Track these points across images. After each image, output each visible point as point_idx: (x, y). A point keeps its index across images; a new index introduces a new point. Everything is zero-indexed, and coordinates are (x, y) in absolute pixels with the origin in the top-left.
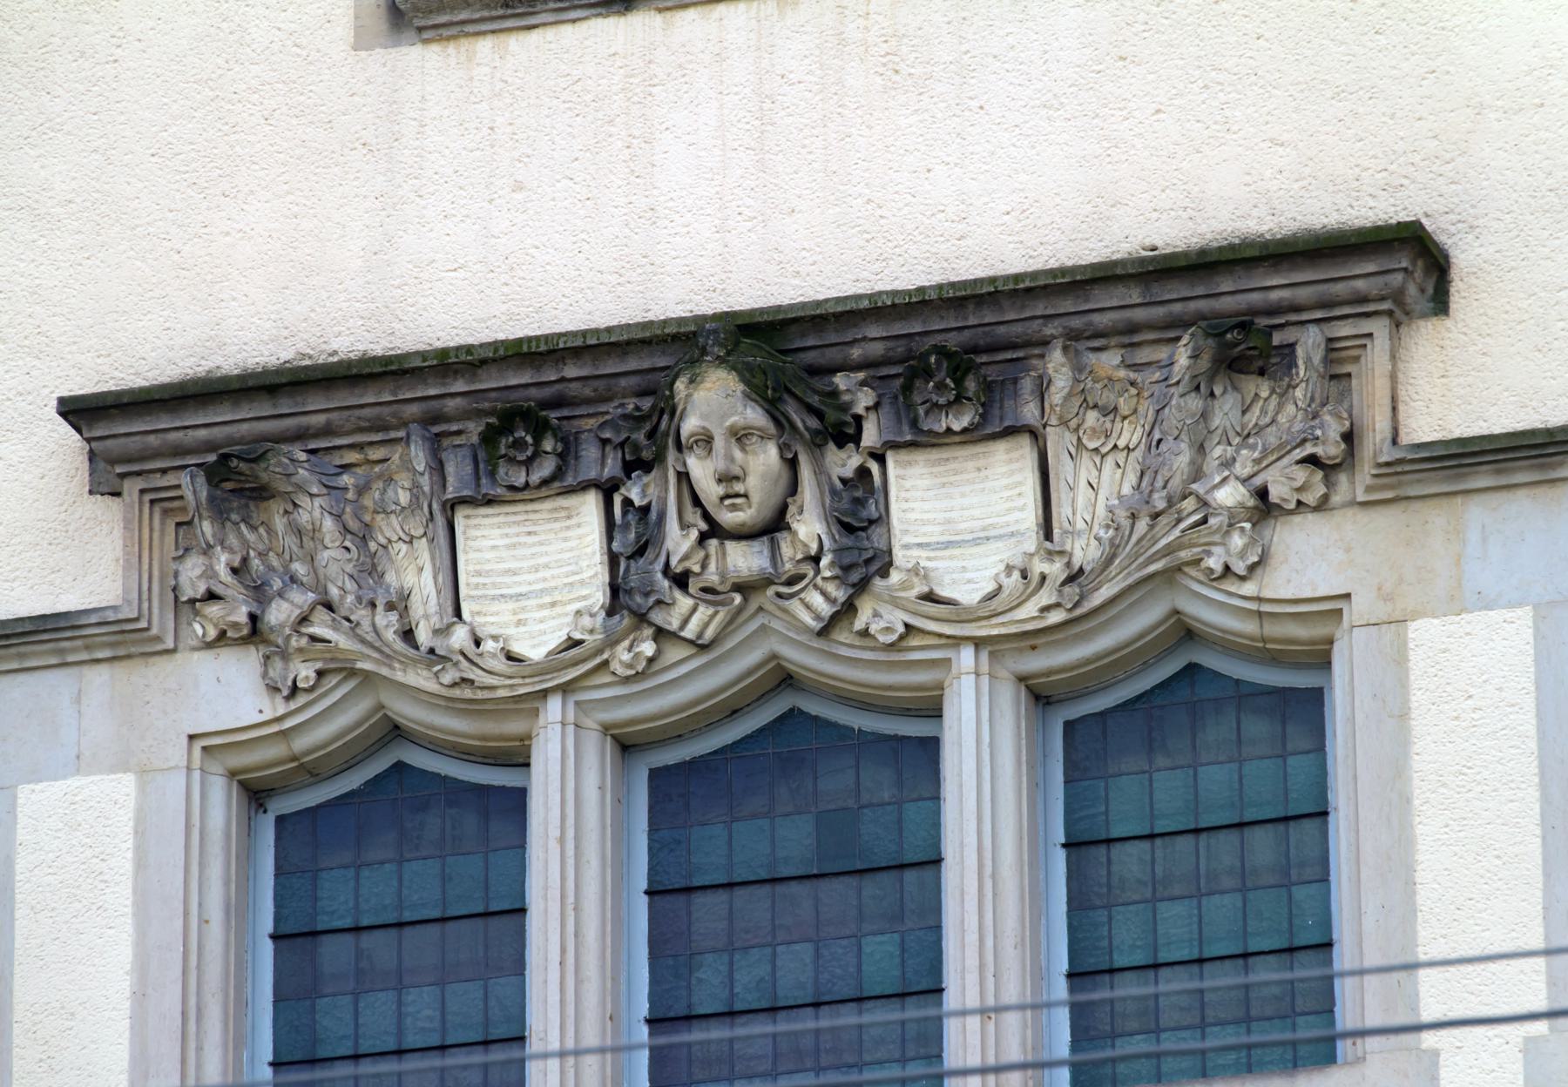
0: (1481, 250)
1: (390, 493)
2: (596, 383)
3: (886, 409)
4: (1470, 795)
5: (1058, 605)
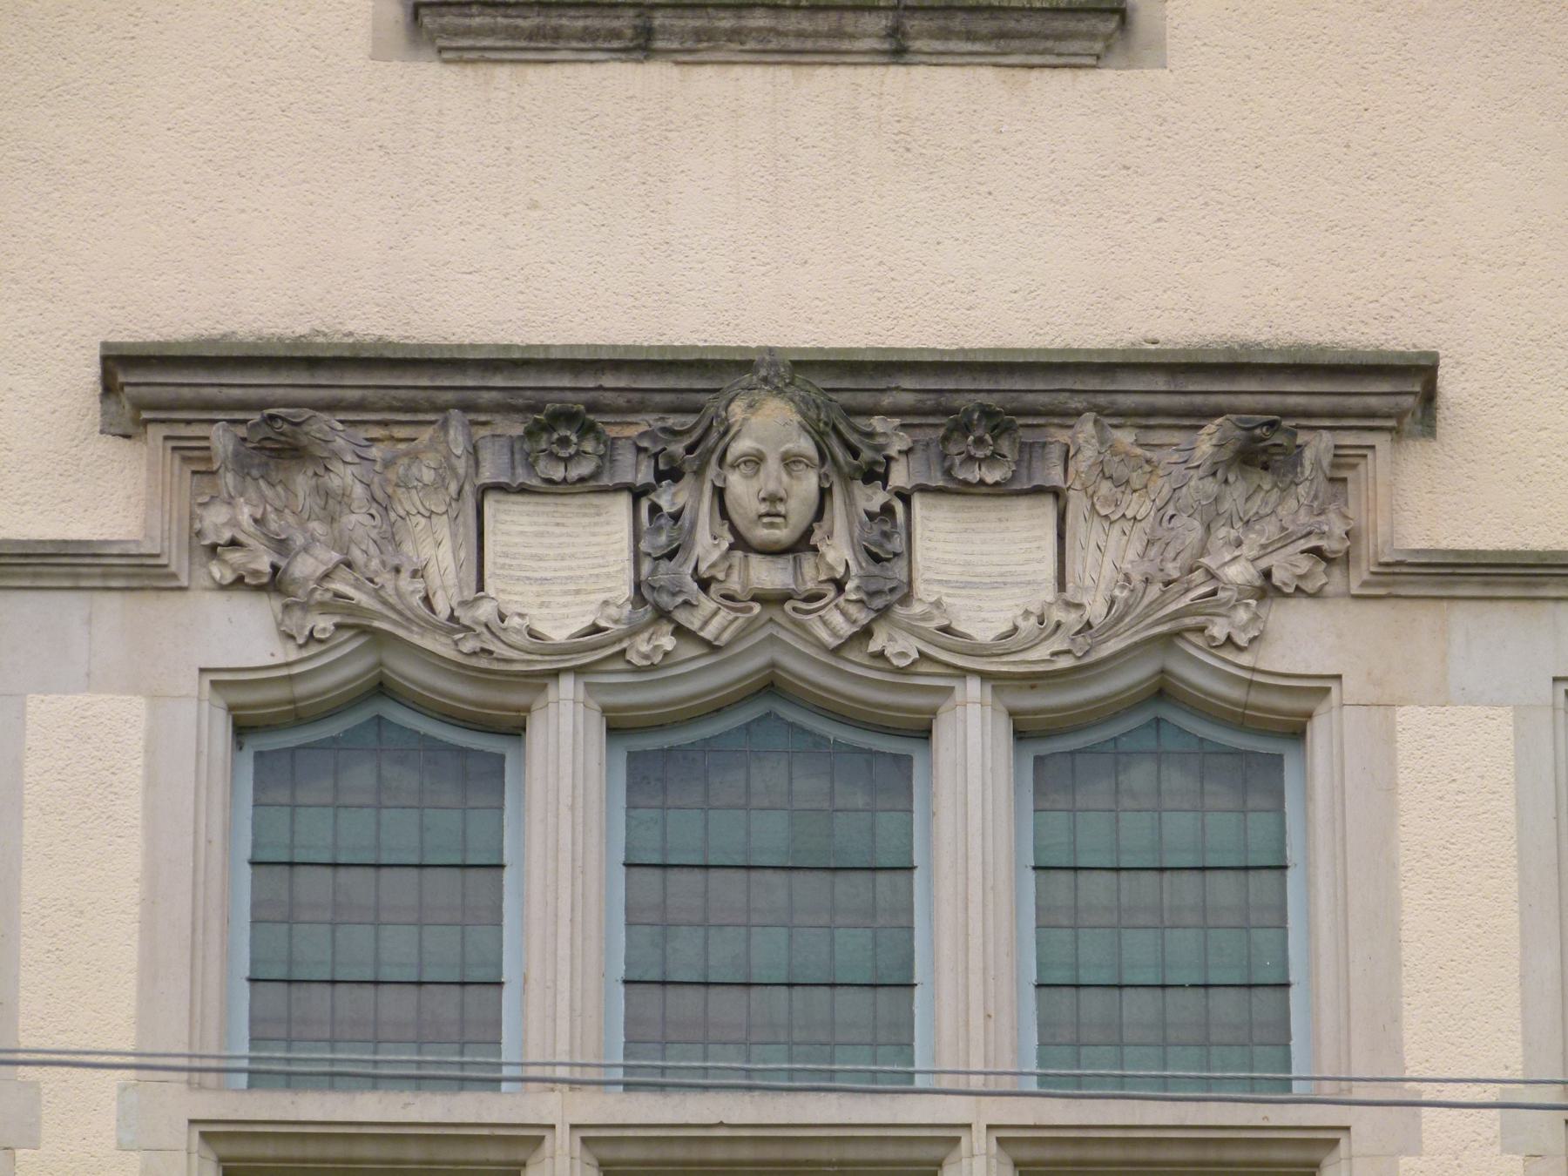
0: (1467, 385)
1: (414, 470)
2: (631, 395)
3: (919, 455)
4: (1454, 868)
5: (1068, 652)
